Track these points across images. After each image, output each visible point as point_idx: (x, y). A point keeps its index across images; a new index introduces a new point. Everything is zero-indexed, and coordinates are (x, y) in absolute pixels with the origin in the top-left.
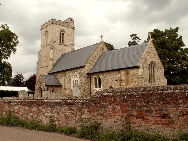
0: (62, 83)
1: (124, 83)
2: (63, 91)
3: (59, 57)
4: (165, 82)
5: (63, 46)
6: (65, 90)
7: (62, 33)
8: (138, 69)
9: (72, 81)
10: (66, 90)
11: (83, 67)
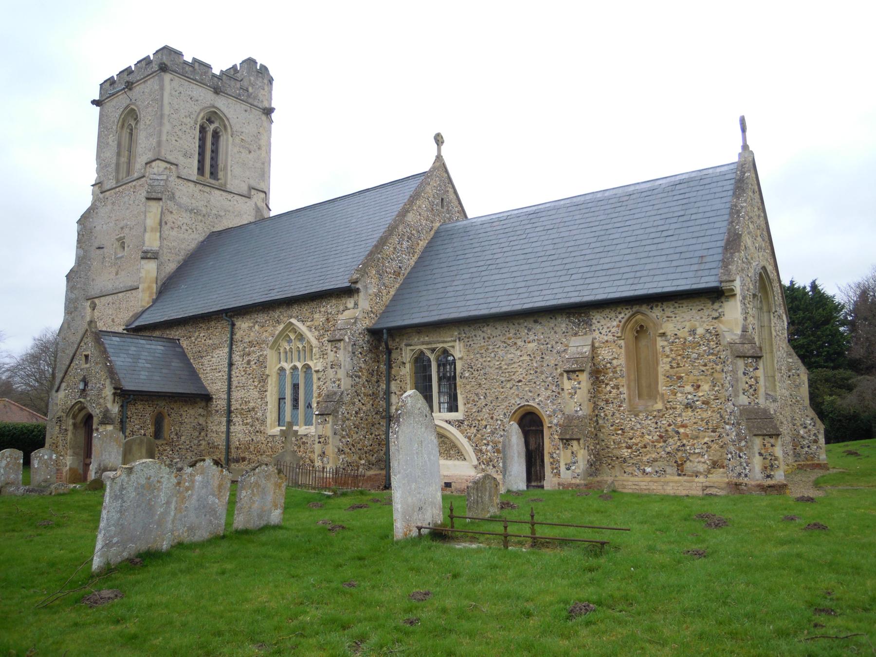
0: (215, 385)
1: (617, 387)
2: (217, 426)
3: (193, 245)
4: (798, 386)
5: (218, 192)
6: (229, 422)
7: (212, 127)
8: (716, 306)
9: (272, 369)
10: (237, 419)
11: (349, 292)
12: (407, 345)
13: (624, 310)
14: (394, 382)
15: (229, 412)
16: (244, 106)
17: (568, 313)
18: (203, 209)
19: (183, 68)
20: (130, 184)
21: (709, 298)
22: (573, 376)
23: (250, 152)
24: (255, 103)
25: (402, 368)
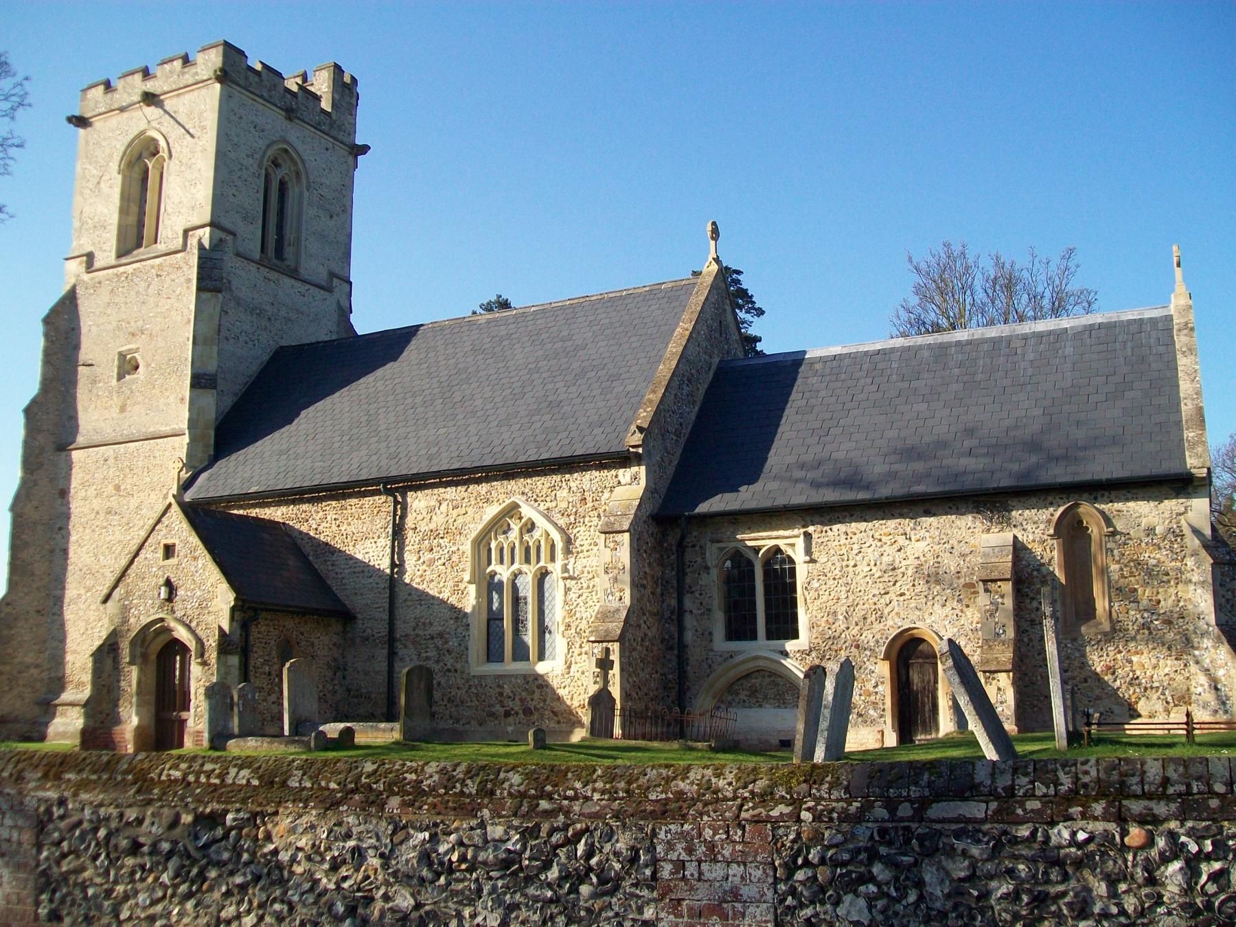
12: (713, 541)
13: (1058, 499)
14: (689, 595)
15: (391, 640)
16: (328, 141)
17: (975, 502)
18: (268, 308)
19: (247, 78)
20: (149, 262)
21: (1172, 489)
22: (992, 586)
23: (331, 217)
24: (340, 137)
25: (704, 576)
